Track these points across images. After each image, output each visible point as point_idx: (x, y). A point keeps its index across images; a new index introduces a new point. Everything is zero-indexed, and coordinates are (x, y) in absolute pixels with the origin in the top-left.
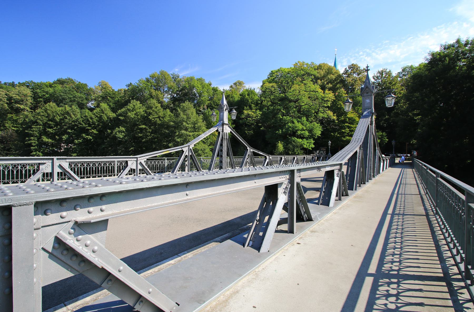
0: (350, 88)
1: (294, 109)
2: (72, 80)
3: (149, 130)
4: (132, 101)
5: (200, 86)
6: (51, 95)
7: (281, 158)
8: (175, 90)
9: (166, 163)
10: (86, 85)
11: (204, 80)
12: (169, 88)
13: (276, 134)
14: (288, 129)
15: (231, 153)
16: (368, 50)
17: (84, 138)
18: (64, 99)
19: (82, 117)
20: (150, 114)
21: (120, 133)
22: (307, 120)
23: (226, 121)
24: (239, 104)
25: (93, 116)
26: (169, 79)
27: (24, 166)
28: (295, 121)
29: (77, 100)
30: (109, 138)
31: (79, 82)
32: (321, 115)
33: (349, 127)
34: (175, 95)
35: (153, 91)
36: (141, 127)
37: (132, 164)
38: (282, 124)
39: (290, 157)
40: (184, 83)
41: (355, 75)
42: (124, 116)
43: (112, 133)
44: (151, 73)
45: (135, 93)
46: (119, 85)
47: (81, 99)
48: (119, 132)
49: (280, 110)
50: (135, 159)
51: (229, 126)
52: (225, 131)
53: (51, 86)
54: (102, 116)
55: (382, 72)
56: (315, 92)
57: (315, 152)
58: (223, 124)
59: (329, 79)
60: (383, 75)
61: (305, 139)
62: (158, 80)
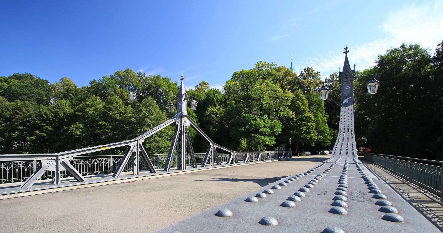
0: (306, 90)
1: (257, 107)
2: (31, 76)
3: (108, 126)
4: (91, 96)
5: (166, 85)
6: (5, 90)
7: (246, 155)
8: (141, 88)
9: (112, 161)
10: (46, 81)
11: (170, 79)
12: (135, 87)
13: (239, 131)
14: (250, 126)
15: (191, 149)
16: (317, 59)
17: (37, 135)
18: (20, 95)
19: (35, 113)
20: (110, 109)
21: (77, 129)
22: (269, 118)
23: (185, 113)
24: (203, 103)
25: (47, 111)
26: (134, 77)
27: (17, 164)
28: (258, 118)
29: (35, 96)
30: (66, 135)
31: (39, 78)
32: (281, 113)
33: (306, 125)
34: (141, 94)
35: (117, 88)
36: (100, 123)
37: (48, 163)
38: (245, 122)
39: (254, 154)
40: (150, 82)
41: (310, 78)
42: (82, 112)
43: (68, 130)
44: (116, 70)
45: (98, 89)
46: (81, 82)
47: (39, 95)
48: (76, 128)
49: (243, 108)
50: (55, 158)
51: (188, 119)
52: (184, 124)
53: (5, 81)
54: (58, 111)
55: (333, 75)
56: (276, 91)
57: (275, 148)
58: (182, 116)
59: (287, 81)
60: (334, 78)
61: (267, 136)
62: (123, 77)
